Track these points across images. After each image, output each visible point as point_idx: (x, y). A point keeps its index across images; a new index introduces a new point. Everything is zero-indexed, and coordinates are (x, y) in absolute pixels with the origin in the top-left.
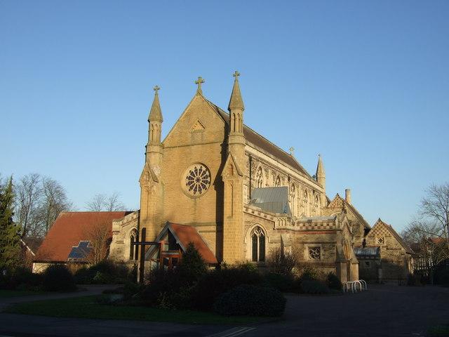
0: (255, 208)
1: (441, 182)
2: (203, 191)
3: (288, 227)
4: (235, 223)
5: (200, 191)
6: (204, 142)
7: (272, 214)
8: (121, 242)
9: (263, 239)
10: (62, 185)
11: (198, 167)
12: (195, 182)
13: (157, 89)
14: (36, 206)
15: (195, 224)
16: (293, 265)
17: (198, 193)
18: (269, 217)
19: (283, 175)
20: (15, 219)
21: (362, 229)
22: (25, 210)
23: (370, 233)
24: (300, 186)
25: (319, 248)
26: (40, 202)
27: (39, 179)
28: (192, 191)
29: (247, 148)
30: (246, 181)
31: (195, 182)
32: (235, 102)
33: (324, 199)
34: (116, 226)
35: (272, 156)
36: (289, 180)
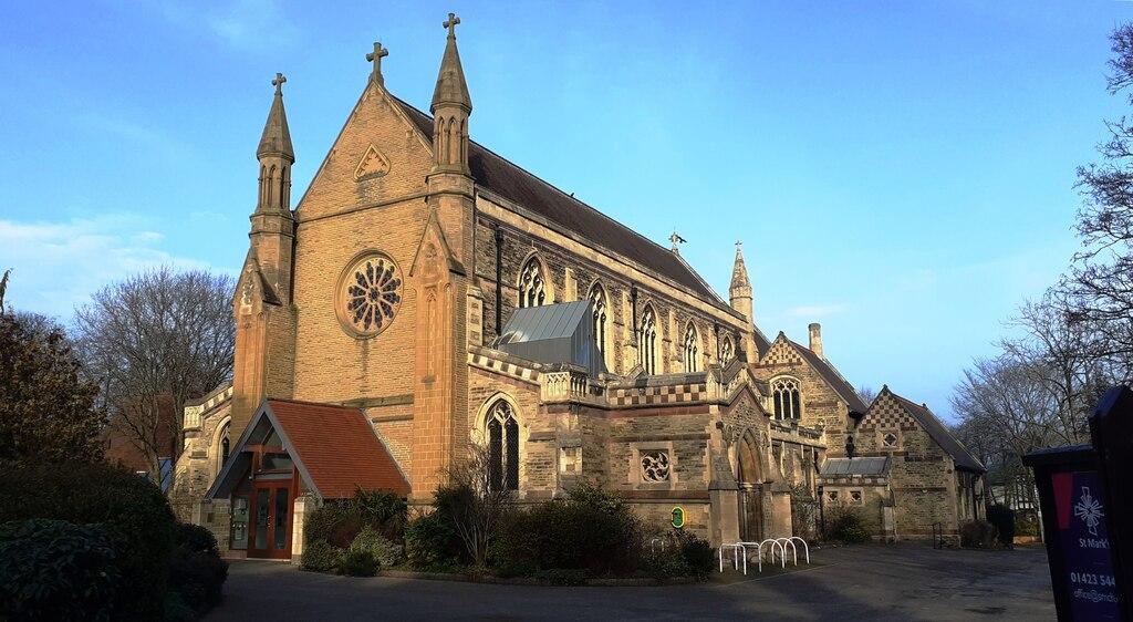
1: (1123, 20)
5: (378, 320)
8: (201, 455)
9: (513, 429)
12: (368, 300)
15: (363, 404)
17: (373, 327)
23: (864, 422)
24: (671, 313)
28: (362, 322)
31: (368, 300)
32: (453, 91)
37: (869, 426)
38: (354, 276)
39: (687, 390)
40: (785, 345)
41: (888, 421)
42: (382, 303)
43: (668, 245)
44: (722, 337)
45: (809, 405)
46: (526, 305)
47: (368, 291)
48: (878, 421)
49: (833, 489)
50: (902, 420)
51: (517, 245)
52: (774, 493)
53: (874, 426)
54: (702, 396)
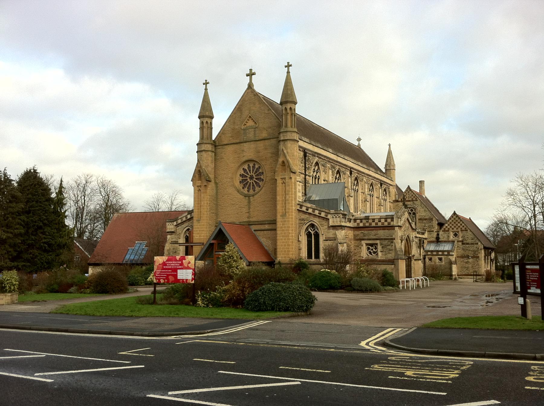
0: (309, 205)
2: (257, 189)
3: (343, 224)
4: (288, 221)
6: (257, 138)
7: (327, 211)
9: (317, 236)
10: (117, 184)
11: (246, 167)
12: (249, 180)
13: (206, 83)
14: (92, 207)
16: (347, 262)
17: (251, 191)
18: (323, 215)
19: (344, 170)
20: (69, 222)
21: (435, 223)
22: (79, 216)
23: (444, 227)
25: (377, 244)
26: (94, 203)
27: (93, 179)
29: (301, 143)
30: (301, 178)
31: (249, 180)
33: (393, 190)
34: (170, 227)
35: (330, 150)
36: (351, 174)
37: (447, 229)
38: (242, 169)
39: (386, 221)
40: (410, 192)
41: (455, 227)
42: (255, 181)
43: (356, 143)
44: (383, 189)
45: (419, 219)
46: (317, 183)
47: (249, 176)
48: (451, 227)
49: (430, 257)
50: (461, 227)
51: (311, 157)
52: (415, 260)
53: (449, 229)
54: (392, 223)
